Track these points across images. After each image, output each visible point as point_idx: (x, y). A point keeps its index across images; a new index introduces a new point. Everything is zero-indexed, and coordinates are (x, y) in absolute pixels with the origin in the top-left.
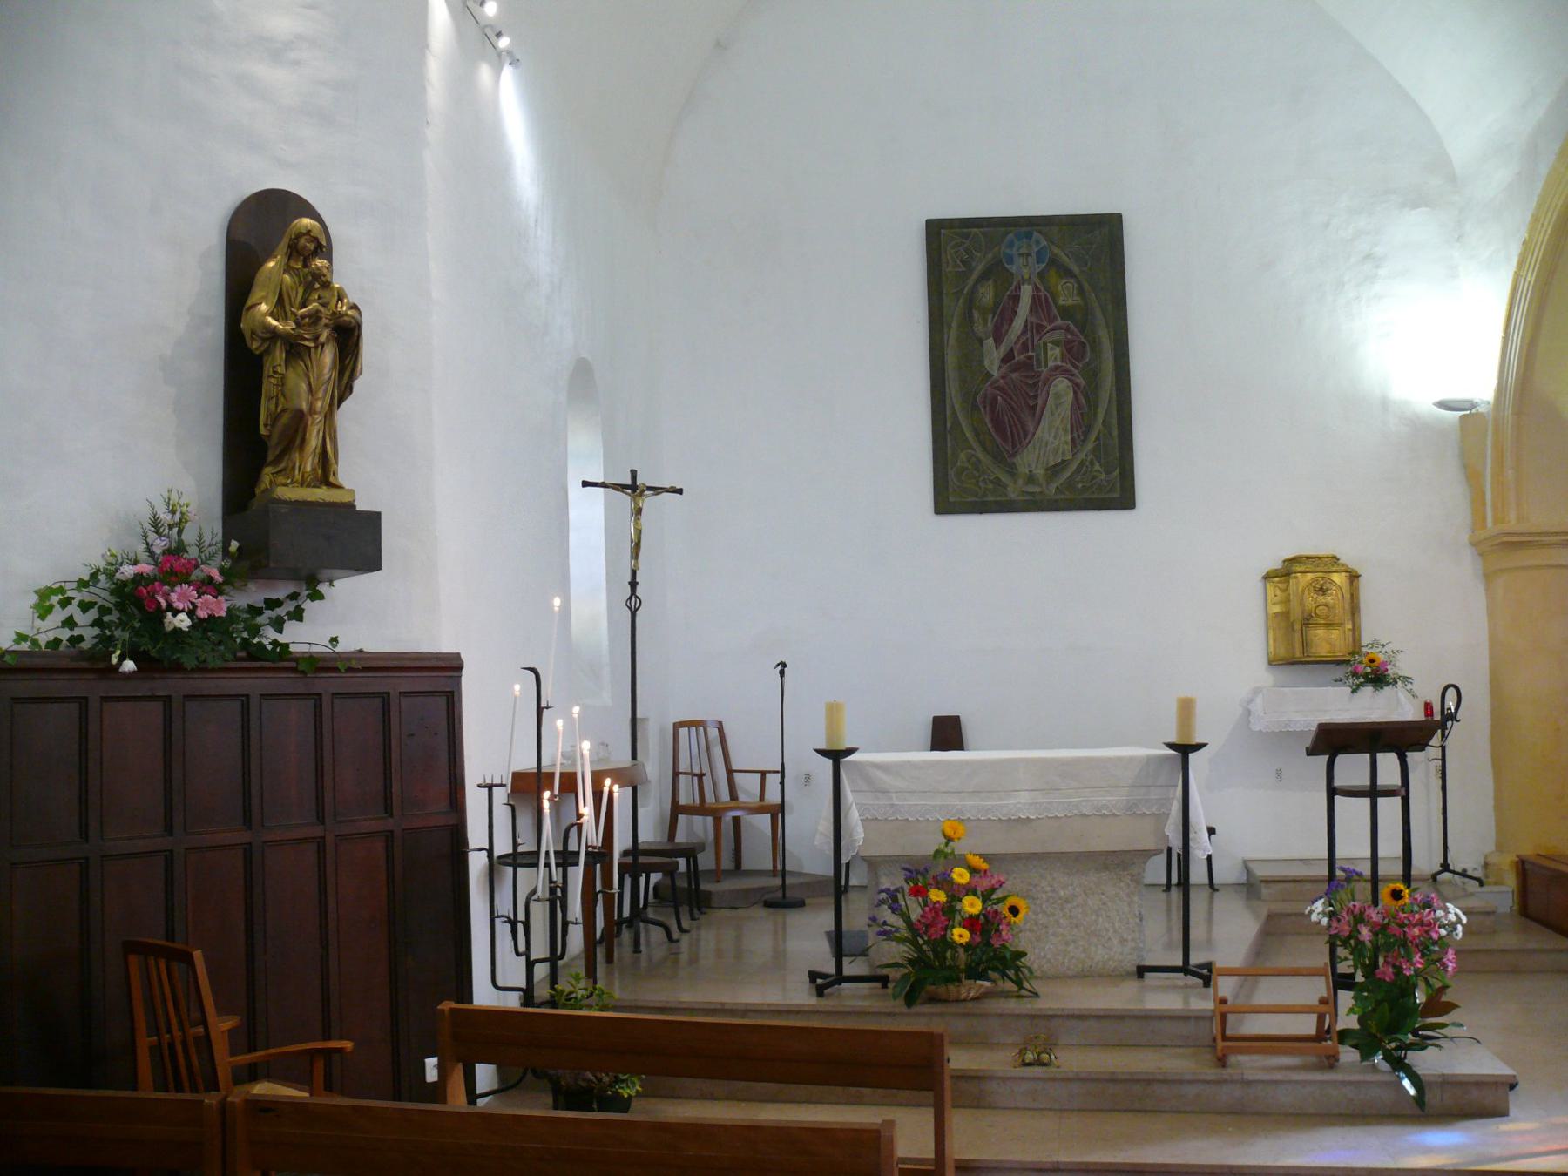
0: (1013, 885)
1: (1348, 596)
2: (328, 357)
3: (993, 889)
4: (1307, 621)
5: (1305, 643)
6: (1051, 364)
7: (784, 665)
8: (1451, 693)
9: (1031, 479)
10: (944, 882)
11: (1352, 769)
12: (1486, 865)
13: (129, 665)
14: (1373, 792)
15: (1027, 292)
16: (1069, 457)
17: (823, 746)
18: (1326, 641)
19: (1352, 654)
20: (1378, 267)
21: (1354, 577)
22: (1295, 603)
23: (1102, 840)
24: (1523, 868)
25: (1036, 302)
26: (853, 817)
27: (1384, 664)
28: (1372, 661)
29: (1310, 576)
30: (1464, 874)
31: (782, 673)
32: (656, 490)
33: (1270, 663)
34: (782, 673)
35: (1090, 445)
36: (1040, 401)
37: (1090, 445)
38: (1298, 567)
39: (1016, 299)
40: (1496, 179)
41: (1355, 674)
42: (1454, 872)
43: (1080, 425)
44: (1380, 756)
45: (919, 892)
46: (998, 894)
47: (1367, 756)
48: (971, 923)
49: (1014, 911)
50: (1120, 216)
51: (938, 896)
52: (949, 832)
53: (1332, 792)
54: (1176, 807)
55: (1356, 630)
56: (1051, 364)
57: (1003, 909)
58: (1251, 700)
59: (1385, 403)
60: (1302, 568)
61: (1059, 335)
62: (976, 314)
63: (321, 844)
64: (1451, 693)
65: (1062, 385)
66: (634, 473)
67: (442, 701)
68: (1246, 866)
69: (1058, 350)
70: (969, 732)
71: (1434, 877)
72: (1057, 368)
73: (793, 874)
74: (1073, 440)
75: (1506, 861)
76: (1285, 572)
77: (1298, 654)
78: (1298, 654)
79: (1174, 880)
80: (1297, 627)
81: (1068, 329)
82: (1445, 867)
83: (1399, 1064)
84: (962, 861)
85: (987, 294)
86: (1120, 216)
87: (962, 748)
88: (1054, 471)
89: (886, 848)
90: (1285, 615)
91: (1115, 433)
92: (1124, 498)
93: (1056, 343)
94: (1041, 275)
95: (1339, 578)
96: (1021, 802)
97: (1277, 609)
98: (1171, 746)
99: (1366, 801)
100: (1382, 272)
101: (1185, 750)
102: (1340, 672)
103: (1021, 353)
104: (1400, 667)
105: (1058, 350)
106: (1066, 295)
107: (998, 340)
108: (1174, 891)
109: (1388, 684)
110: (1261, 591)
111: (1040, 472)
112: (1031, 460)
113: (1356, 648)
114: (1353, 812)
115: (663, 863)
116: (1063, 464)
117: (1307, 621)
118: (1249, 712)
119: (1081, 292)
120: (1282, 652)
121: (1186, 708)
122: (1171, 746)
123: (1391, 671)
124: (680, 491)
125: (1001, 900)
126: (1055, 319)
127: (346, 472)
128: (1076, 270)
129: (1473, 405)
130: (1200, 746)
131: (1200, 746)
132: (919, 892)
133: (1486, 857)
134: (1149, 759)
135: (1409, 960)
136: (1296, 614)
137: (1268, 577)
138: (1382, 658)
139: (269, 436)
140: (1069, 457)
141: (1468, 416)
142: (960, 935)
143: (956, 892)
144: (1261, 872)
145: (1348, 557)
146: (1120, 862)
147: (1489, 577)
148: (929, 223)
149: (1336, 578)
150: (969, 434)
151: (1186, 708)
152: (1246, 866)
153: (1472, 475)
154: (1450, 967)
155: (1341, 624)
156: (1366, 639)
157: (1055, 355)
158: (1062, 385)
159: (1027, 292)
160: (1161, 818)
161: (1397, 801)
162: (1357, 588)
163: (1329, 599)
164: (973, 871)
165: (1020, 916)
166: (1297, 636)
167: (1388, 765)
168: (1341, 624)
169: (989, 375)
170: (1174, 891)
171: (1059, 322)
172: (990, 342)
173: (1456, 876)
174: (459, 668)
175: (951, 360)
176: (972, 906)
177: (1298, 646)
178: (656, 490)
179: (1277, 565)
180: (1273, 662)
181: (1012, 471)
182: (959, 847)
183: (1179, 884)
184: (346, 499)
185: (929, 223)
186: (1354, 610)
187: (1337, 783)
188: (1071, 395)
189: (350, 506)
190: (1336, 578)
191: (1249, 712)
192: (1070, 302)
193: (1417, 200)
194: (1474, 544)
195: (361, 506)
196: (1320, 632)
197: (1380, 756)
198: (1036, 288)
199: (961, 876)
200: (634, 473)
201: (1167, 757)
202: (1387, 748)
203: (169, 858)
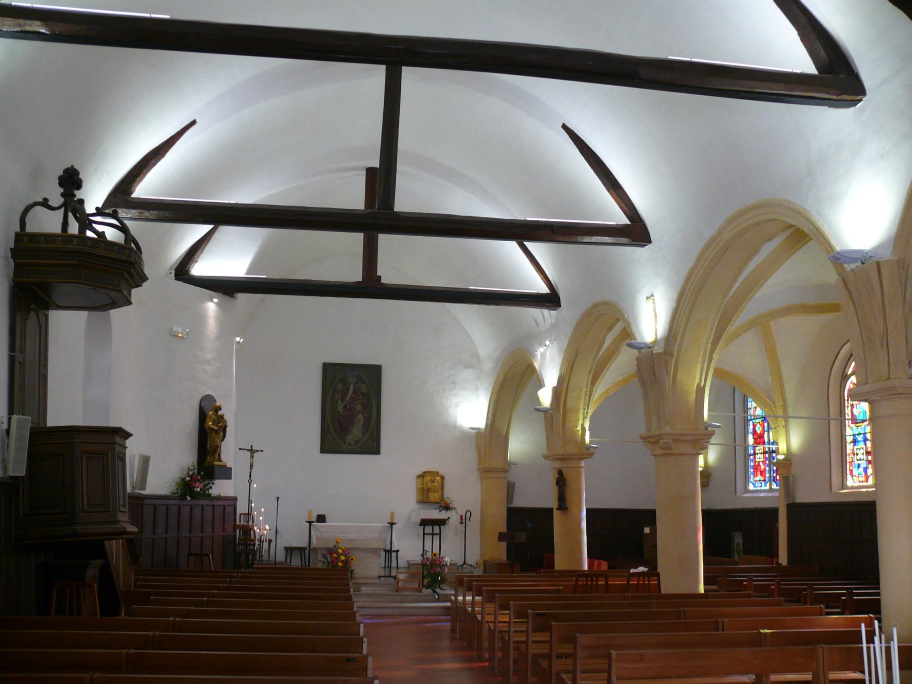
0: (352, 555)
1: (440, 483)
2: (221, 434)
3: (347, 555)
4: (428, 490)
5: (427, 497)
6: (358, 409)
7: (278, 498)
8: (469, 513)
9: (350, 444)
10: (337, 552)
11: (428, 529)
12: (477, 564)
13: (189, 498)
14: (433, 534)
15: (352, 387)
16: (361, 438)
17: (307, 520)
18: (434, 496)
19: (441, 500)
20: (455, 385)
21: (443, 478)
22: (425, 485)
23: (372, 545)
24: (485, 562)
25: (354, 392)
26: (313, 537)
27: (449, 504)
28: (446, 503)
29: (430, 477)
30: (471, 565)
31: (278, 500)
32: (257, 451)
33: (417, 502)
34: (278, 500)
35: (368, 434)
36: (354, 421)
37: (368, 434)
38: (427, 475)
39: (348, 389)
40: (488, 365)
41: (441, 507)
42: (467, 565)
43: (365, 428)
44: (434, 526)
45: (331, 554)
46: (349, 555)
47: (431, 526)
48: (342, 562)
49: (352, 559)
50: (381, 366)
51: (335, 555)
52: (338, 541)
53: (424, 534)
54: (389, 538)
55: (442, 494)
56: (358, 409)
57: (350, 559)
58: (411, 513)
59: (455, 426)
60: (428, 475)
61: (361, 401)
62: (336, 393)
63: (213, 537)
64: (469, 513)
65: (360, 416)
66: (252, 446)
67: (233, 507)
68: (408, 562)
69: (360, 406)
70: (327, 519)
71: (462, 565)
72: (359, 411)
73: (264, 561)
74: (363, 433)
75: (481, 562)
76: (422, 476)
77: (425, 500)
78: (425, 500)
79: (387, 566)
80: (426, 492)
81: (363, 399)
82: (465, 563)
83: (435, 592)
84: (340, 548)
85: (340, 387)
86: (381, 366)
87: (325, 522)
88: (357, 442)
89: (321, 546)
90: (422, 488)
91: (375, 431)
92: (376, 450)
93: (360, 403)
94: (356, 382)
95: (438, 478)
96: (353, 536)
97: (420, 486)
98: (389, 523)
99: (431, 536)
100: (457, 387)
101: (392, 524)
102: (437, 506)
103: (349, 405)
104: (454, 505)
105: (360, 406)
106: (364, 390)
107: (342, 402)
108: (387, 569)
109: (450, 510)
110: (415, 481)
111: (352, 442)
112: (350, 438)
113: (442, 499)
114: (428, 539)
115: (585, 474)
116: (360, 440)
117: (428, 490)
118: (410, 517)
119: (368, 388)
120: (421, 499)
121: (392, 514)
122: (389, 523)
123: (451, 505)
124: (262, 451)
125: (348, 557)
126: (360, 396)
127: (223, 457)
128: (367, 382)
129: (479, 429)
130: (395, 523)
131: (395, 523)
132: (331, 554)
133: (477, 561)
134: (383, 526)
135: (437, 568)
136: (425, 488)
137: (418, 477)
138: (449, 502)
139: (209, 450)
140: (361, 438)
141: (478, 432)
142: (340, 564)
143: (339, 555)
144: (411, 562)
145: (441, 472)
146: (375, 551)
147: (482, 479)
148: (324, 364)
149: (437, 478)
150: (332, 430)
151: (392, 514)
152: (408, 562)
153: (479, 449)
154: (446, 571)
155: (438, 492)
156: (445, 496)
157: (359, 407)
158: (360, 416)
159: (352, 387)
160: (385, 541)
161: (438, 536)
162: (444, 482)
163: (435, 484)
164: (343, 551)
165: (354, 560)
166: (425, 495)
167: (436, 529)
168: (438, 492)
169: (339, 412)
170: (387, 569)
171: (361, 397)
172: (340, 402)
173: (468, 566)
174: (237, 500)
175: (328, 407)
176: (343, 558)
177: (425, 497)
178: (257, 451)
179: (421, 473)
180: (419, 502)
181: (344, 442)
182: (340, 545)
183: (388, 567)
184: (225, 464)
185: (324, 364)
186: (442, 488)
187: (425, 532)
188: (363, 419)
189: (225, 466)
190: (437, 478)
191: (410, 517)
192: (365, 391)
193: (468, 366)
194: (478, 469)
195: (228, 466)
196: (432, 494)
197: (434, 526)
198: (355, 386)
199: (340, 551)
200: (252, 446)
201: (386, 526)
202: (429, 525)
203: (213, 537)
